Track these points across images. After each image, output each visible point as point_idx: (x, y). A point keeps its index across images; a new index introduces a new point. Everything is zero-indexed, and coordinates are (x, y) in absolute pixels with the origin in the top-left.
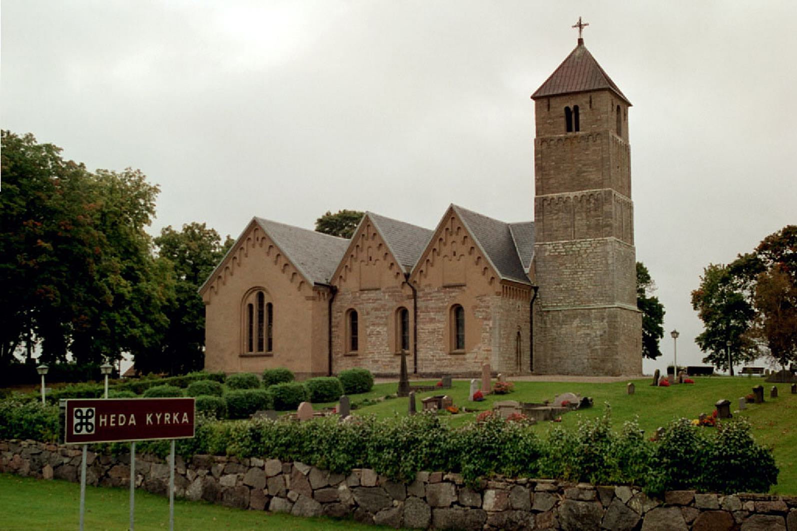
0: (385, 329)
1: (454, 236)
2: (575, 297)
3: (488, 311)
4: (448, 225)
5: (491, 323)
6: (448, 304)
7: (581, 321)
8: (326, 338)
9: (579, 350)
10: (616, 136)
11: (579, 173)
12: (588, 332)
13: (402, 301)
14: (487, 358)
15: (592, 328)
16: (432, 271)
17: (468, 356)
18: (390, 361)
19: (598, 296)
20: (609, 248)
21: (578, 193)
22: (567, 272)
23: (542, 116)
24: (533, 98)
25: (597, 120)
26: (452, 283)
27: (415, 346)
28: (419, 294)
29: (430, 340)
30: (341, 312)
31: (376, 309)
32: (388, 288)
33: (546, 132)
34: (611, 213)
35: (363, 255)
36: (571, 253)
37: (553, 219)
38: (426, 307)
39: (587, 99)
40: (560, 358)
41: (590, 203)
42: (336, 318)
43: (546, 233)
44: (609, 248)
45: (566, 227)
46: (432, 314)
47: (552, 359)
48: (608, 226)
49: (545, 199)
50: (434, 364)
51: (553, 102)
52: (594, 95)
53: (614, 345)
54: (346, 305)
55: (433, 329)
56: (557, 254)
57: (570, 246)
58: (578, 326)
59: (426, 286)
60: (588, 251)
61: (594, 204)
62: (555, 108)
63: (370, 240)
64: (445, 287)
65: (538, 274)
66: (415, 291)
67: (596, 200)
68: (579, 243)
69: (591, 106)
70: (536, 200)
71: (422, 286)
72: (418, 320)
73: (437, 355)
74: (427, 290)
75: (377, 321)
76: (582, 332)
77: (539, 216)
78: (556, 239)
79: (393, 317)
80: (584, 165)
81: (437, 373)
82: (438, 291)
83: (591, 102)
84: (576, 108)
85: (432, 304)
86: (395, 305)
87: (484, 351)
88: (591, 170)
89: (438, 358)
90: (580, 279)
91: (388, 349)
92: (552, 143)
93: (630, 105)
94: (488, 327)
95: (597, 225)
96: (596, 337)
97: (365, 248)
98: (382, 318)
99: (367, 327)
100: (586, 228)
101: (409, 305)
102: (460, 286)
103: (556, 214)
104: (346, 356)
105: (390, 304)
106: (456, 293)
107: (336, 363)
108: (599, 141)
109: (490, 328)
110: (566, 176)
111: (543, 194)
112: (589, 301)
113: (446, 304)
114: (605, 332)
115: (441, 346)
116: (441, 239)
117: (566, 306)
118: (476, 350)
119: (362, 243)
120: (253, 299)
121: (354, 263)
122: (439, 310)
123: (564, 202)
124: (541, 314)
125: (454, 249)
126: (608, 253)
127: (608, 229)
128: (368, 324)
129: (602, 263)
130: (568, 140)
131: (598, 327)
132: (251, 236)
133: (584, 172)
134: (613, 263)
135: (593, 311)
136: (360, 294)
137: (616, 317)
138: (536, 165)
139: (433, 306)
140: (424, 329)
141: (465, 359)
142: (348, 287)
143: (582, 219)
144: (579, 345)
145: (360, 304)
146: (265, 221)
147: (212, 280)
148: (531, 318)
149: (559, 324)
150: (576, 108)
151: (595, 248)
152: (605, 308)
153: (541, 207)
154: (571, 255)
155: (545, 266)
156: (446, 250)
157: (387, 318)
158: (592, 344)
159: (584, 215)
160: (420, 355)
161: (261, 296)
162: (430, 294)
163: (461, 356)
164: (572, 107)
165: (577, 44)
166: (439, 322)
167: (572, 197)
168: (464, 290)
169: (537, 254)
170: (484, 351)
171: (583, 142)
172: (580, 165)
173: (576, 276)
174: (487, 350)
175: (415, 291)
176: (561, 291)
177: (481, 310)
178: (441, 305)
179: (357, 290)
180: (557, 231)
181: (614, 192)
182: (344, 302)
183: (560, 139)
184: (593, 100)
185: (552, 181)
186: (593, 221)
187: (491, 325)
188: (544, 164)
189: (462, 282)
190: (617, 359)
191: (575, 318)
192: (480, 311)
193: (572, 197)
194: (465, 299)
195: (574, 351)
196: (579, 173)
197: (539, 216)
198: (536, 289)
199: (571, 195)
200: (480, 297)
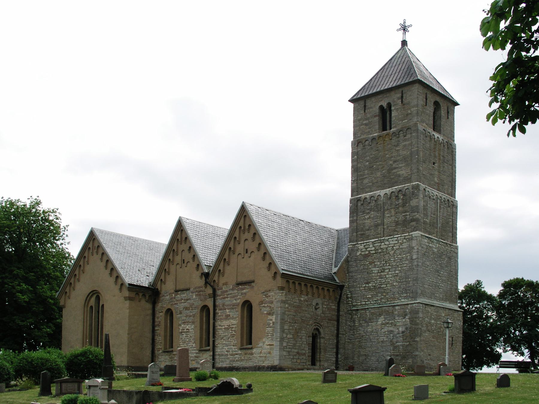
0: (193, 327)
1: (246, 233)
2: (382, 295)
3: (272, 306)
4: (241, 224)
5: (273, 318)
6: (240, 301)
7: (385, 318)
8: (150, 335)
9: (382, 347)
10: (431, 130)
11: (390, 170)
12: (391, 329)
13: (206, 299)
14: (270, 353)
15: (395, 325)
16: (228, 269)
17: (254, 350)
18: (195, 357)
19: (402, 293)
20: (414, 243)
21: (388, 191)
22: (375, 270)
23: (359, 118)
24: (351, 101)
25: (407, 115)
26: (244, 279)
27: (214, 341)
28: (219, 292)
29: (225, 336)
30: (162, 312)
31: (186, 308)
32: (196, 288)
33: (362, 134)
34: (417, 207)
35: (178, 259)
36: (380, 251)
37: (365, 219)
38: (223, 305)
39: (399, 95)
40: (365, 355)
41: (399, 199)
42: (158, 318)
43: (359, 233)
44: (414, 243)
45: (377, 226)
46: (227, 311)
47: (359, 356)
48: (412, 220)
49: (359, 200)
50: (228, 358)
51: (369, 103)
52: (405, 89)
53: (414, 341)
54: (165, 306)
55: (229, 323)
56: (367, 252)
57: (379, 244)
58: (382, 324)
59: (224, 284)
60: (395, 248)
61: (403, 199)
62: (371, 108)
63: (183, 243)
64: (239, 284)
65: (351, 274)
66: (214, 291)
67: (404, 195)
68: (388, 240)
69: (402, 103)
70: (351, 201)
71: (221, 284)
72: (217, 317)
73: (231, 350)
74: (224, 289)
75: (187, 319)
76: (386, 329)
77: (353, 217)
78: (368, 238)
79: (198, 315)
80: (395, 162)
81: (230, 367)
82: (233, 289)
83: (402, 97)
84: (389, 105)
85: (228, 301)
86: (200, 304)
87: (268, 345)
88: (400, 165)
89: (231, 353)
90: (387, 276)
91: (194, 345)
92: (367, 143)
93: (457, 104)
94: (271, 322)
95: (405, 221)
96: (399, 334)
97: (180, 252)
98: (190, 316)
99: (180, 325)
100: (394, 224)
101: (210, 303)
102: (249, 283)
103: (369, 213)
104: (164, 352)
105: (196, 304)
106: (246, 290)
107: (158, 358)
108: (408, 136)
109: (273, 323)
110: (379, 174)
111: (358, 195)
112: (394, 298)
113: (238, 301)
114: (406, 329)
115: (234, 342)
116: (235, 238)
117: (373, 304)
118: (261, 345)
119: (177, 248)
120: (93, 301)
121: (171, 266)
122: (233, 307)
123: (376, 201)
124: (352, 312)
125: (246, 248)
126: (413, 248)
127: (414, 223)
128: (180, 323)
129: (407, 259)
130: (381, 139)
131: (400, 324)
132: (90, 246)
133: (395, 168)
134: (418, 258)
135: (397, 308)
136: (176, 295)
137: (417, 312)
138: (352, 167)
139: (229, 303)
140: (222, 324)
141: (252, 354)
142: (167, 288)
143: (391, 216)
144: (382, 342)
145: (176, 304)
146: (102, 232)
147: (65, 287)
148: (338, 316)
149: (366, 322)
150: (389, 105)
151: (401, 244)
152: (408, 304)
153: (357, 207)
154: (380, 253)
155: (357, 266)
156: (240, 249)
157: (194, 316)
158: (395, 340)
159: (393, 211)
160: (218, 351)
161: (98, 298)
162: (227, 291)
163: (249, 351)
164: (385, 105)
165: (400, 46)
166: (233, 318)
167: (382, 195)
168: (253, 287)
169: (350, 254)
170: (268, 345)
171: (394, 138)
172: (391, 162)
173: (383, 274)
174: (270, 345)
175: (214, 291)
176: (370, 289)
177: (266, 305)
178: (235, 302)
179: (173, 291)
180: (368, 230)
181: (422, 186)
182: (163, 305)
183: (374, 139)
184: (404, 95)
185: (366, 181)
186: (401, 218)
187: (274, 320)
188: (359, 165)
189: (251, 278)
190: (416, 355)
191: (380, 315)
192: (264, 307)
193: (382, 195)
194: (252, 294)
195: (378, 348)
196: (390, 170)
197: (353, 217)
198: (342, 287)
199: (382, 193)
200: (265, 293)
